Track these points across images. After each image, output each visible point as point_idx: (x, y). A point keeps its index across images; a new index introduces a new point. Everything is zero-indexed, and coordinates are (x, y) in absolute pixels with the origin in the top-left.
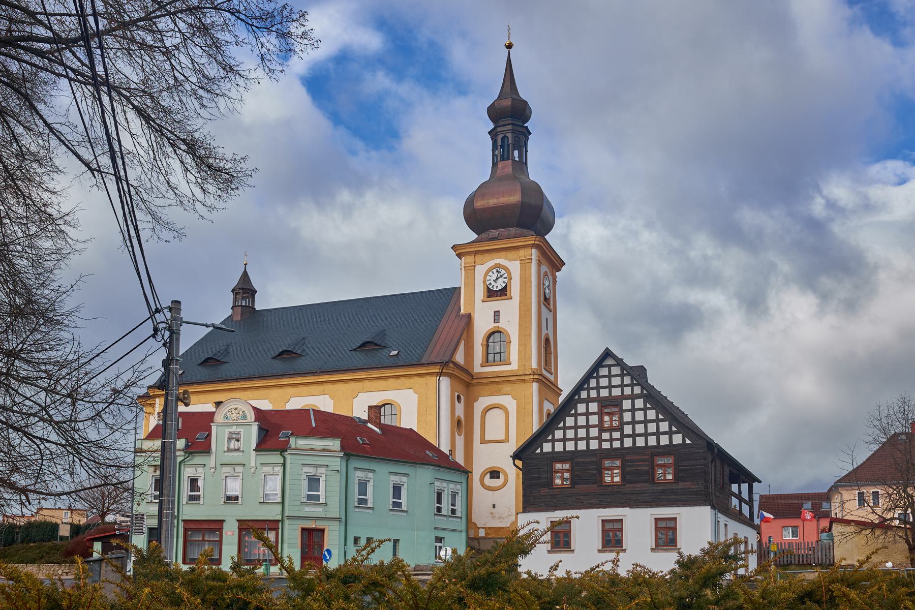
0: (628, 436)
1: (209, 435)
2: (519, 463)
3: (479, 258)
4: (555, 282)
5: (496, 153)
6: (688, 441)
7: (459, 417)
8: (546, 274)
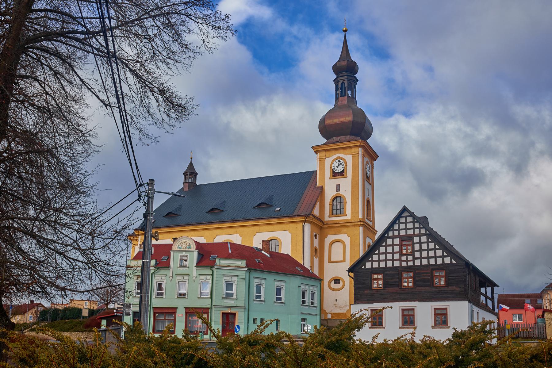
0: (417, 258)
1: (169, 258)
2: (352, 274)
3: (328, 153)
4: (373, 167)
5: (338, 92)
6: (454, 262)
7: (316, 247)
8: (367, 163)
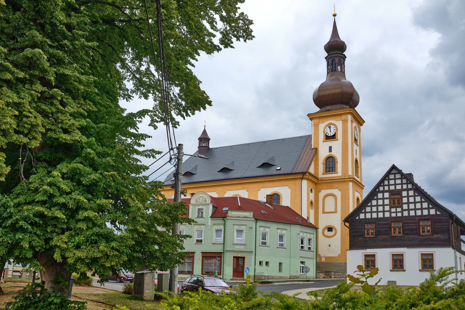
0: (405, 210)
2: (347, 224)
3: (321, 120)
6: (438, 213)
7: (311, 200)
8: (355, 127)
